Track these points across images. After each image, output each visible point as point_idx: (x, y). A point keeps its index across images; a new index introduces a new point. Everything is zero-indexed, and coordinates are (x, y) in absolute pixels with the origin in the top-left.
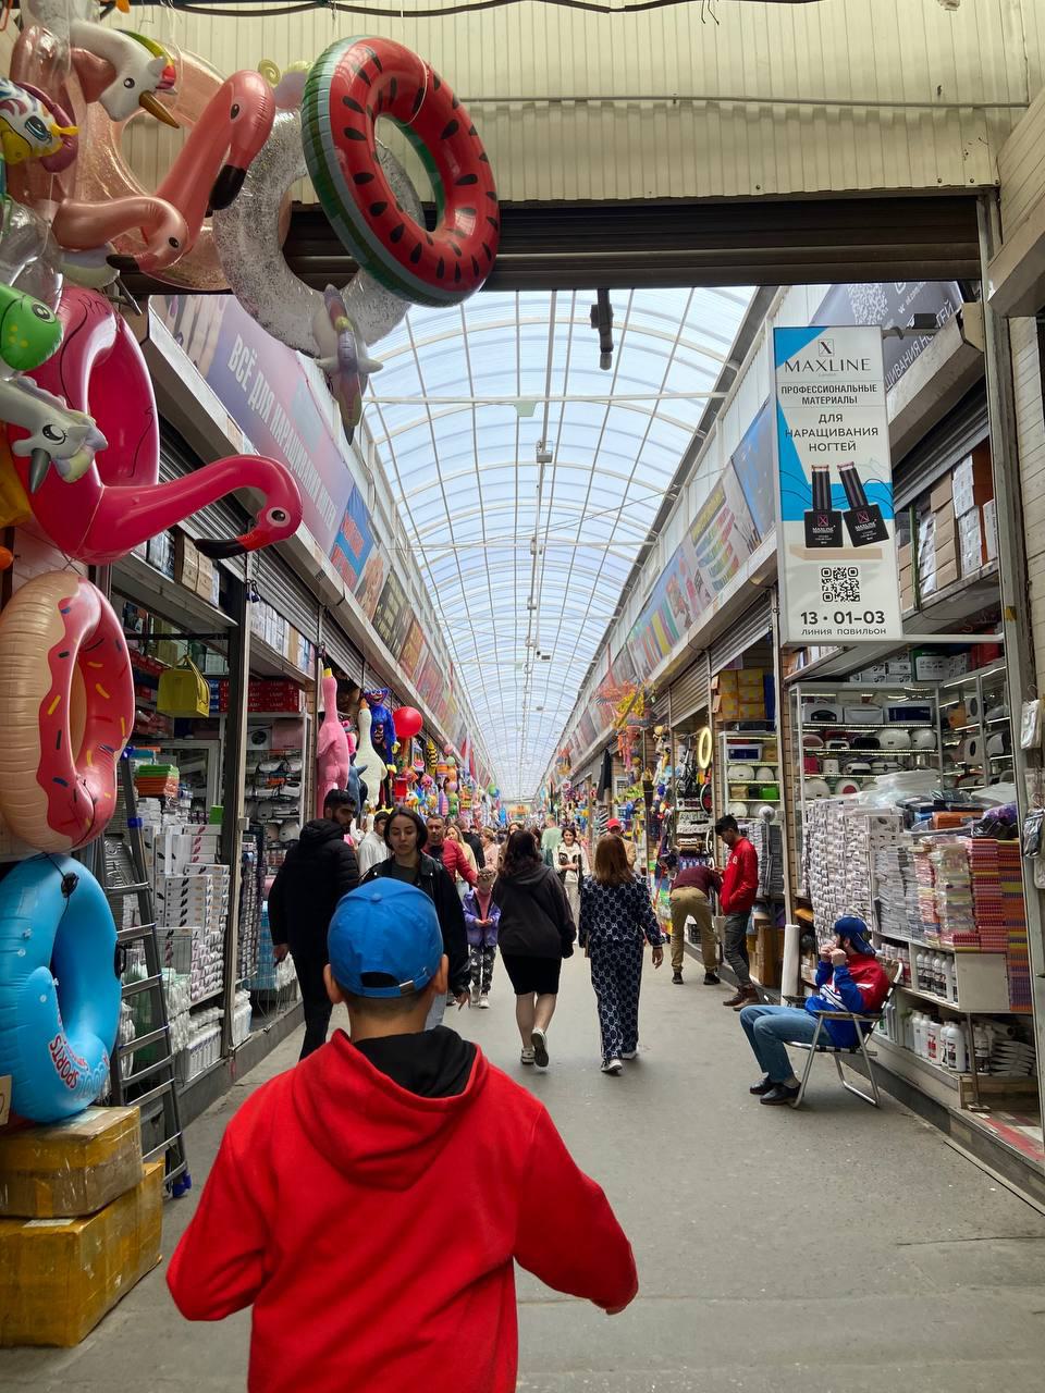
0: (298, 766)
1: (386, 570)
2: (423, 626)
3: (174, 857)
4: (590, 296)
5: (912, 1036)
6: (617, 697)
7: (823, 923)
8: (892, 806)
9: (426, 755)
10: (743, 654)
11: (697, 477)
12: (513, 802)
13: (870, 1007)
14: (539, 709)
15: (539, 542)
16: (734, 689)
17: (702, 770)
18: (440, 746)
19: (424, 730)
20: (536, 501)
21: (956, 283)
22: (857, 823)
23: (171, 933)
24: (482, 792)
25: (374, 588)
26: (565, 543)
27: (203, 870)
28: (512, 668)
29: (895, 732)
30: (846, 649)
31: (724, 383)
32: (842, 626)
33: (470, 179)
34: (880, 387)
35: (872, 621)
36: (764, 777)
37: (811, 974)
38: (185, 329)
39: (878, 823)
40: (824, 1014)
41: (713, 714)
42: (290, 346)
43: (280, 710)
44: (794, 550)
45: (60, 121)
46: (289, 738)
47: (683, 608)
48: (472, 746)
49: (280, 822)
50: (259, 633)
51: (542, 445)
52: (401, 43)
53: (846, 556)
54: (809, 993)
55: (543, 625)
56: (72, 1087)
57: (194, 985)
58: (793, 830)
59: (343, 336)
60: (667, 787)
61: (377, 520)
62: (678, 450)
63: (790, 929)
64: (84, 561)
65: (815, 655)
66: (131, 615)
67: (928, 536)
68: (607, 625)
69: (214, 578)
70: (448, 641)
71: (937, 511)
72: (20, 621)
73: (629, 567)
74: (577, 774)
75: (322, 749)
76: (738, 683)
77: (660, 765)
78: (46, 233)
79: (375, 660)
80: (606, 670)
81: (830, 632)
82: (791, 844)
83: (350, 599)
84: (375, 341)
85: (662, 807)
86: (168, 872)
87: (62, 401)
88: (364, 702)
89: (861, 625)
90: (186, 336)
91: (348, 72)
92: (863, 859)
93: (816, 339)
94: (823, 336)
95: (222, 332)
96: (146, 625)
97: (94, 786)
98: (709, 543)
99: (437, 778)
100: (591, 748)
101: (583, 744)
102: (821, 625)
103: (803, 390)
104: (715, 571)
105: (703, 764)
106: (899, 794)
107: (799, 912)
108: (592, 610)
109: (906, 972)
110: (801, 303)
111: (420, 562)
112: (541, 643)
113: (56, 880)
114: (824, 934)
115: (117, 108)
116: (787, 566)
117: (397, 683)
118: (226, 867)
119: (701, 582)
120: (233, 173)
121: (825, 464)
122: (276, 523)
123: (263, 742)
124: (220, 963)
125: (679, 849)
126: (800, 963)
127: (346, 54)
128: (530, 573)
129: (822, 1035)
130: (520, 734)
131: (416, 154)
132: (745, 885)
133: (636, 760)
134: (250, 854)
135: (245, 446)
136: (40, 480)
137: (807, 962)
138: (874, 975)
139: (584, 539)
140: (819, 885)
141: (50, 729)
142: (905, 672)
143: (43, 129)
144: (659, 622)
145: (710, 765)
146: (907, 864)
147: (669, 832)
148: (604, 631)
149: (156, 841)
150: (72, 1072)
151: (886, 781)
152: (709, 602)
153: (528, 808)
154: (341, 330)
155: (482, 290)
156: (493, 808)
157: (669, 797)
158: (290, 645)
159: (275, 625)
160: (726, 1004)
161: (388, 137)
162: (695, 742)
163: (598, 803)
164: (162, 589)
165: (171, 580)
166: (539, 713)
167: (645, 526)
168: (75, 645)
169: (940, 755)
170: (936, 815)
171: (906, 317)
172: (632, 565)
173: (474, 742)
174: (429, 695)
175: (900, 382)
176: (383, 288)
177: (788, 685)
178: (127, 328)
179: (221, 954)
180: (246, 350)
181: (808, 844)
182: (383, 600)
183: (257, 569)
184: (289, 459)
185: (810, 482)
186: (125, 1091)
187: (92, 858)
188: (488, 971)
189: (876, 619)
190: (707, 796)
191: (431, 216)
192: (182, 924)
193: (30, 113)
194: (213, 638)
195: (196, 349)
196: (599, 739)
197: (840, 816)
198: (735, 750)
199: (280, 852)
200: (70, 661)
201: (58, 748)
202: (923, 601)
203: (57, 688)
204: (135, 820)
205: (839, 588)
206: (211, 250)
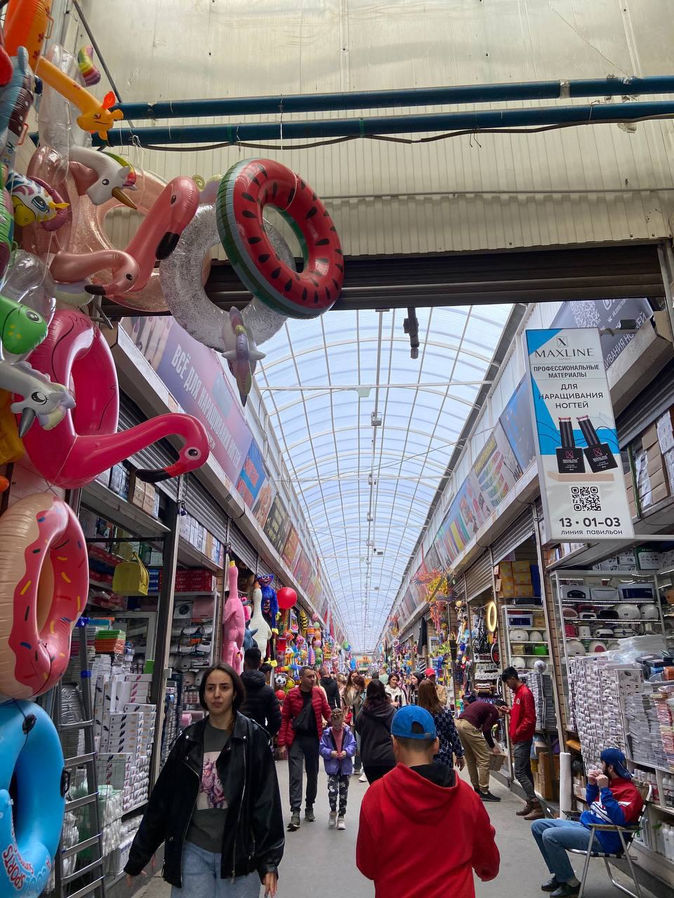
0: (210, 630)
1: (273, 495)
2: (299, 532)
3: (117, 699)
4: (403, 313)
5: (663, 844)
6: (429, 581)
7: (588, 752)
8: (633, 662)
9: (300, 621)
10: (515, 549)
11: (476, 433)
12: (359, 654)
13: (629, 820)
14: (377, 588)
15: (374, 477)
16: (511, 575)
17: (491, 633)
18: (310, 614)
19: (298, 604)
20: (371, 451)
21: (646, 299)
22: (608, 675)
23: (111, 757)
24: (339, 647)
25: (266, 506)
26: (393, 477)
27: (137, 709)
28: (358, 560)
29: (628, 607)
30: (589, 546)
31: (491, 374)
32: (590, 528)
33: (326, 242)
34: (601, 366)
35: (611, 525)
36: (536, 639)
37: (583, 793)
38: (144, 340)
39: (624, 675)
40: (596, 827)
41: (497, 592)
42: (207, 346)
43: (199, 590)
44: (551, 475)
45: (56, 200)
46: (203, 610)
47: (472, 519)
48: (332, 615)
49: (196, 671)
50: (185, 536)
51: (375, 414)
52: (282, 163)
53: (587, 481)
54: (581, 807)
55: (377, 531)
56: (19, 888)
57: (125, 798)
58: (561, 679)
59: (239, 337)
60: (466, 645)
61: (269, 464)
62: (463, 417)
63: (564, 756)
64: (61, 486)
65: (567, 550)
66: (102, 526)
67: (642, 466)
68: (420, 532)
69: (156, 499)
70: (316, 543)
71: (648, 450)
72: (9, 527)
73: (434, 493)
74: (403, 635)
75: (226, 618)
76: (512, 570)
77: (461, 629)
78: (45, 273)
79: (265, 556)
80: (420, 561)
81: (581, 532)
82: (560, 690)
83: (249, 514)
84: (263, 342)
85: (464, 660)
86: (112, 710)
87: (48, 377)
88: (257, 584)
89: (603, 527)
90: (144, 344)
91: (246, 179)
92: (615, 702)
93: (555, 336)
94: (559, 335)
95: (168, 342)
96: (112, 533)
97: (53, 648)
98: (487, 475)
99: (307, 638)
100: (412, 617)
101: (407, 613)
102: (574, 527)
103: (548, 369)
104: (493, 493)
105: (492, 628)
106: (638, 653)
107: (569, 743)
108: (410, 521)
109: (655, 792)
110: (544, 314)
111: (297, 490)
112: (376, 544)
113: (20, 720)
114: (589, 760)
115: (98, 197)
116: (547, 486)
117: (280, 570)
118: (154, 706)
119: (483, 501)
120: (172, 235)
121: (568, 417)
122: (192, 458)
123: (187, 612)
124: (147, 780)
125: (477, 691)
126: (573, 783)
127: (246, 169)
128: (368, 497)
129: (594, 843)
130: (364, 606)
131: (289, 227)
132: (526, 721)
133: (444, 625)
134: (172, 696)
135: (176, 409)
136: (25, 432)
137: (578, 782)
138: (632, 795)
139: (403, 474)
140: (584, 722)
141: (21, 605)
142: (631, 563)
143: (44, 204)
144: (455, 527)
145: (496, 629)
146: (650, 708)
147: (469, 679)
148: (418, 535)
149: (106, 686)
150: (19, 876)
151: (626, 644)
152: (489, 515)
153: (370, 658)
154: (239, 333)
155: (331, 310)
156: (346, 659)
157: (468, 653)
158: (206, 544)
159: (197, 531)
160: (518, 814)
161: (272, 220)
162: (485, 613)
163: (418, 656)
164: (119, 506)
165: (126, 501)
166: (376, 592)
167: (443, 466)
168: (46, 544)
169: (662, 623)
170: (666, 669)
171: (614, 322)
172: (435, 492)
173: (333, 611)
174: (302, 578)
175: (613, 365)
176: (268, 308)
177: (549, 572)
178: (102, 337)
179: (147, 774)
180: (184, 354)
181: (573, 690)
182: (272, 514)
183: (186, 493)
184: (210, 422)
185: (558, 429)
186: (64, 887)
187: (51, 703)
188: (343, 797)
189: (614, 523)
190: (496, 651)
191: (299, 265)
192: (120, 751)
193: (36, 194)
194: (154, 540)
195: (151, 352)
196: (418, 609)
197: (596, 669)
198: (514, 619)
199: (195, 693)
200: (41, 556)
201: (26, 620)
202: (643, 512)
203: (30, 575)
204: (86, 672)
205: (585, 501)
206: (157, 287)
